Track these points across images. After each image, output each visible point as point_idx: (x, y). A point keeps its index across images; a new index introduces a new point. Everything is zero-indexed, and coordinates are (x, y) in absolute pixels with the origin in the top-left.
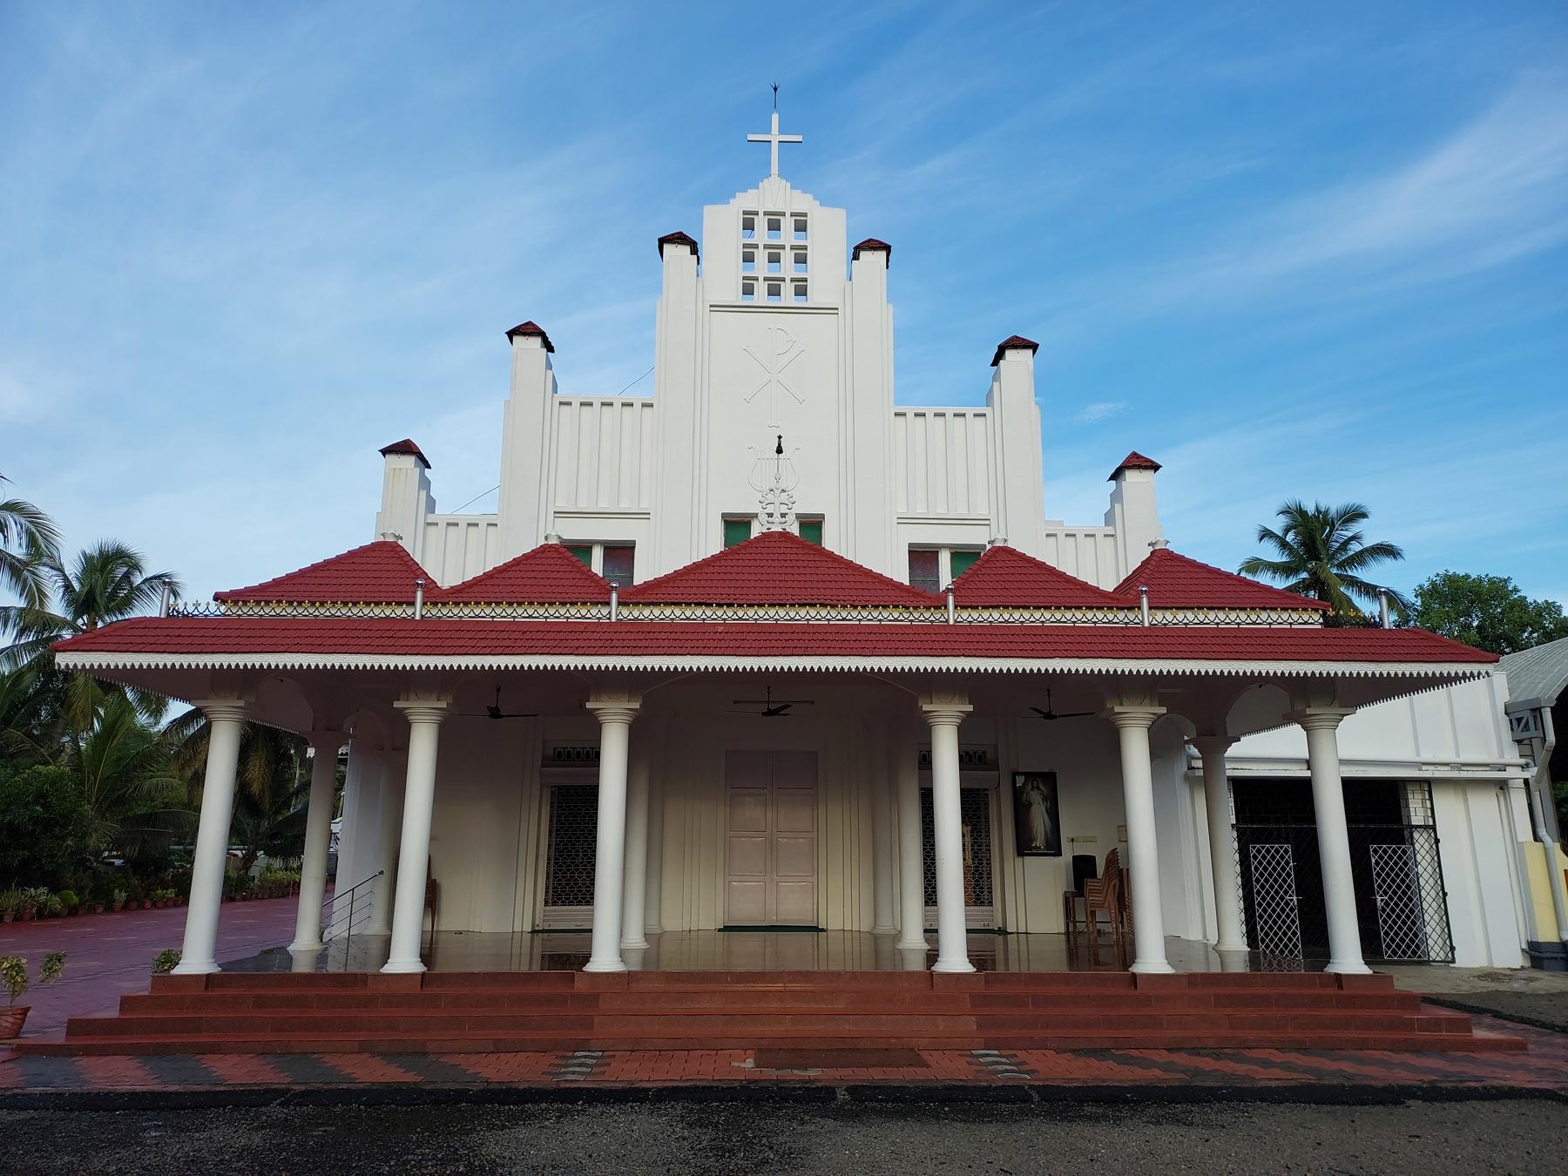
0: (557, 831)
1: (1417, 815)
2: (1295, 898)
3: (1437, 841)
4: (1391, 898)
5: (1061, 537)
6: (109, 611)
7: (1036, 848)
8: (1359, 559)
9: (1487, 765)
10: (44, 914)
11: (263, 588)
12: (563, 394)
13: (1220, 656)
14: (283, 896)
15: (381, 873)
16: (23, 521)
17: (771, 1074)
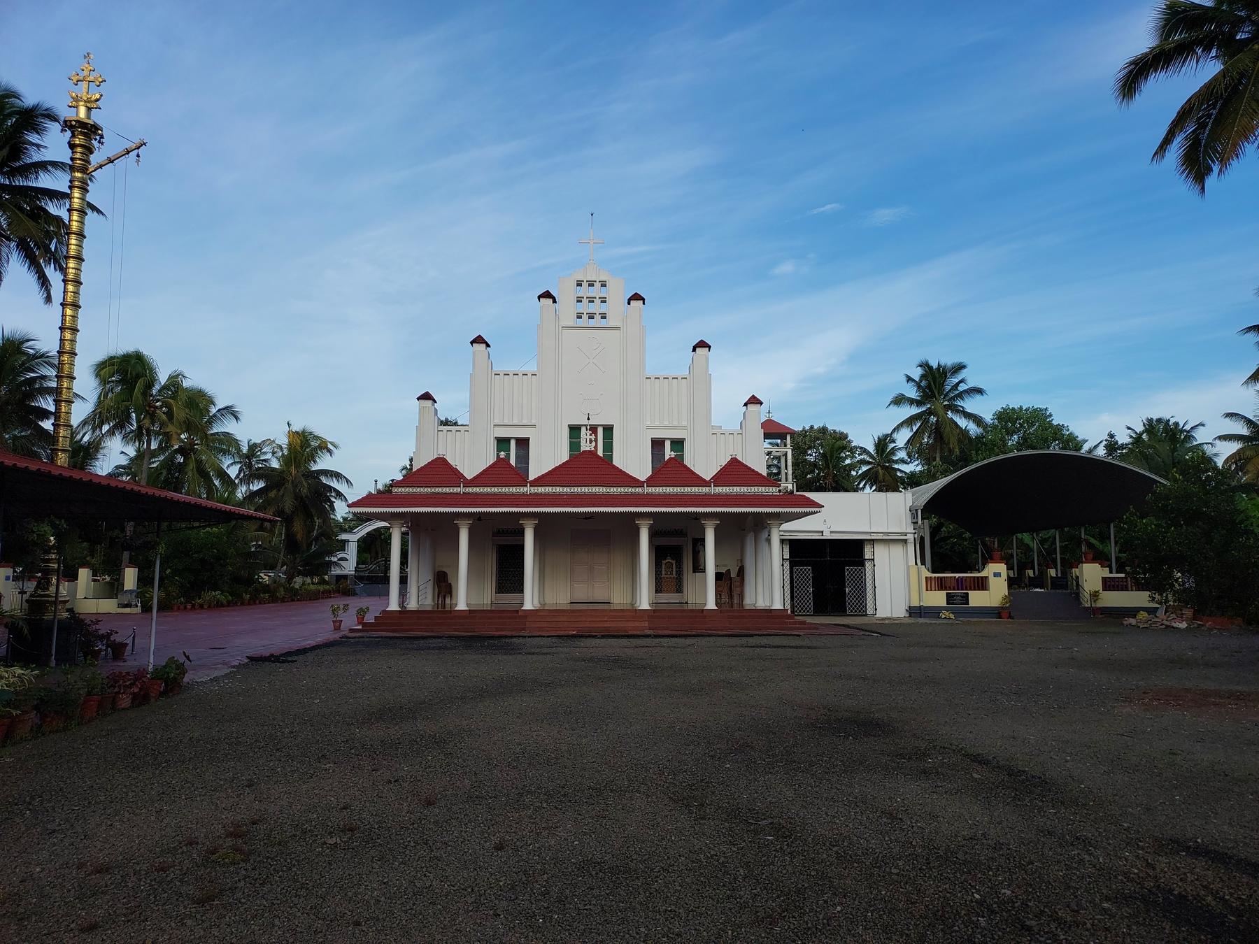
1: (868, 555)
3: (874, 565)
4: (852, 589)
8: (961, 396)
10: (220, 605)
12: (496, 369)
14: (317, 599)
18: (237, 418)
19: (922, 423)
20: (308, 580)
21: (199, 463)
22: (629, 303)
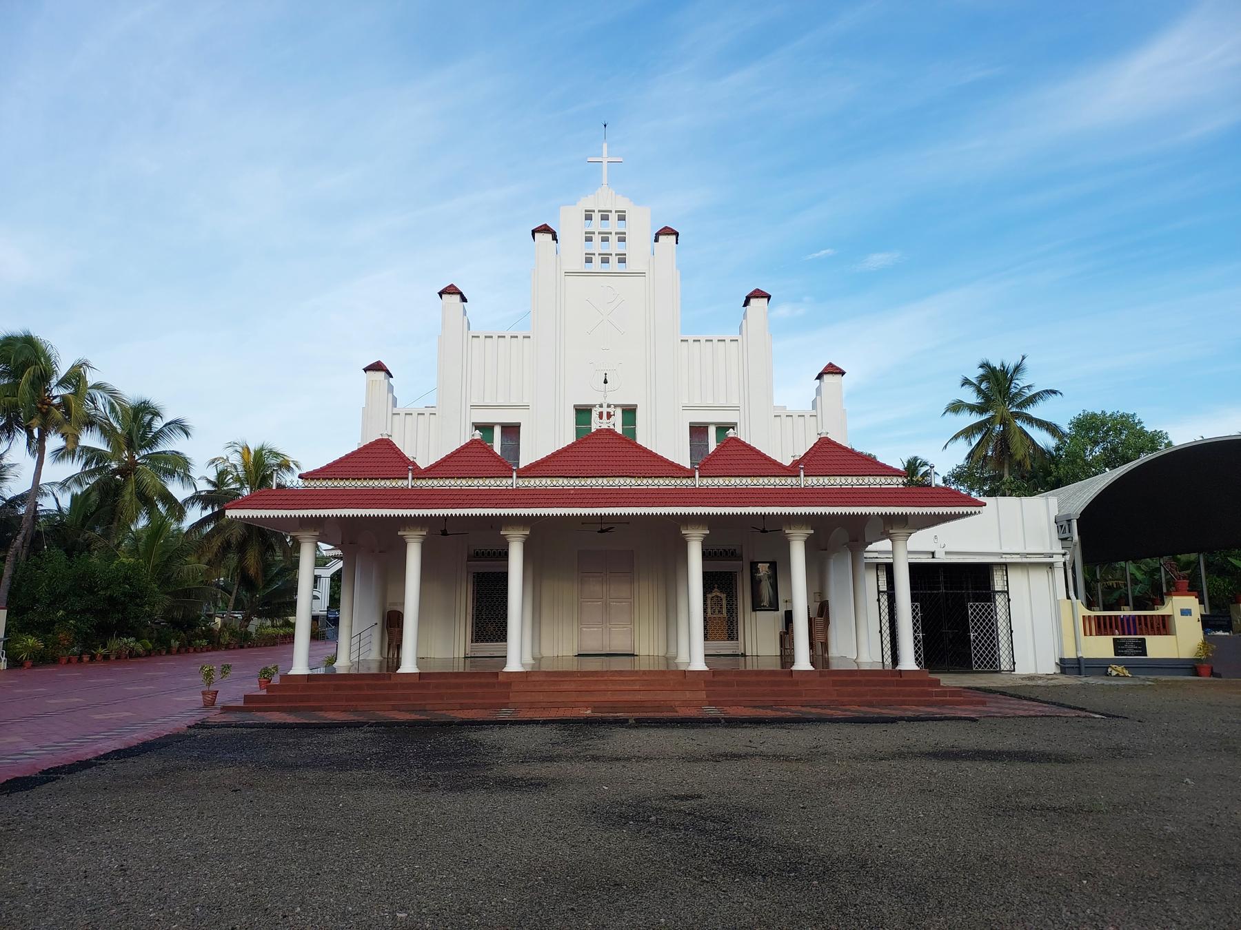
0: (477, 599)
1: (998, 584)
2: (921, 635)
3: (1009, 600)
4: (979, 635)
5: (783, 417)
6: (142, 447)
7: (764, 606)
8: (1032, 400)
9: (1042, 554)
10: (133, 655)
11: (322, 470)
12: (473, 331)
13: (837, 504)
14: (274, 645)
15: (376, 624)
16: (106, 395)
17: (597, 714)
18: (187, 434)
19: (983, 438)
20: (269, 623)
21: (138, 483)
22: (656, 240)
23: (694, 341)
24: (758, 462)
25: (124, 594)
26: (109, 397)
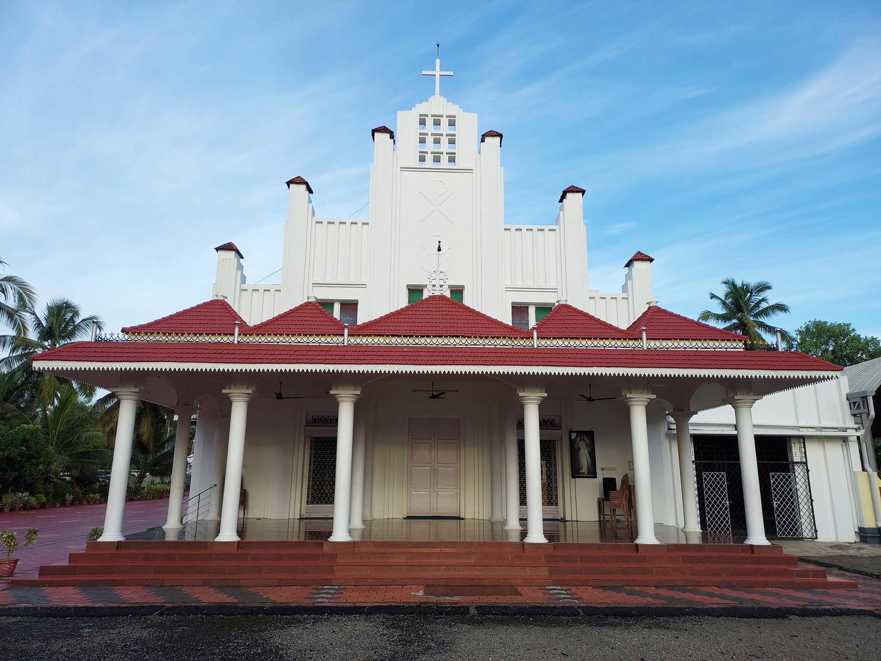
2: (728, 502)
3: (808, 471)
7: (582, 473)
8: (765, 312)
9: (836, 428)
10: (27, 507)
12: (318, 217)
14: (161, 498)
15: (215, 485)
16: (16, 287)
17: (433, 599)
23: (516, 230)
24: (594, 326)
25: (22, 455)
26: (19, 289)
